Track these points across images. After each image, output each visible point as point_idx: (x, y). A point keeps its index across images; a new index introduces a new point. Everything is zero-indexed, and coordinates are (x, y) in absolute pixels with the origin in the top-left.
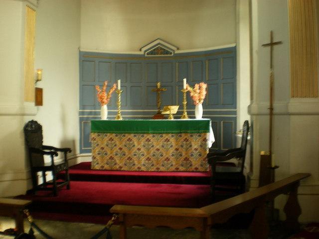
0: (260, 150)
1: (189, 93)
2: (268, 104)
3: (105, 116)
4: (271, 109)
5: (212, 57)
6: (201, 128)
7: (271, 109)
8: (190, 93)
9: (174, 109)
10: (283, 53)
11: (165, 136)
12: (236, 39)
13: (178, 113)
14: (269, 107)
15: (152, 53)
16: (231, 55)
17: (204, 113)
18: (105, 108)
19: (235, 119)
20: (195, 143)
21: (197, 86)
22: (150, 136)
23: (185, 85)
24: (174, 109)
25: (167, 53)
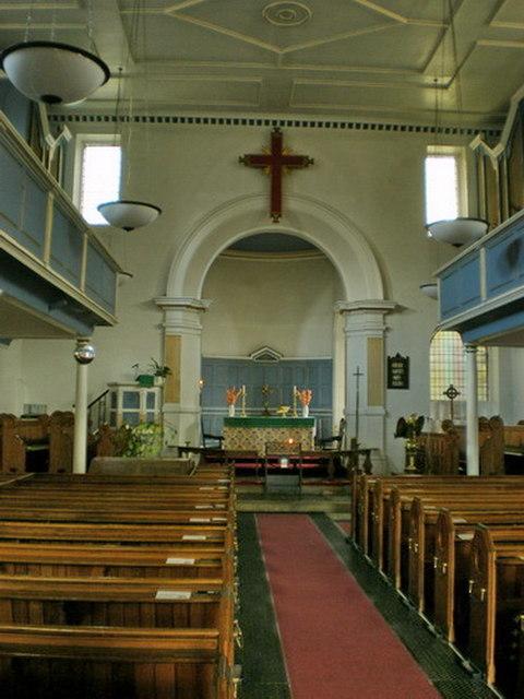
0: (350, 434)
1: (298, 397)
2: (214, 434)
3: (232, 415)
4: (357, 412)
5: (311, 366)
6: (308, 423)
7: (357, 412)
8: (451, 422)
9: (286, 409)
10: (364, 380)
11: (282, 430)
12: (333, 352)
13: (289, 411)
14: (439, 107)
15: (259, 358)
16: (328, 366)
17: (310, 412)
18: (307, 409)
19: (331, 418)
20: (304, 435)
21: (304, 393)
22: (270, 430)
23: (295, 391)
24: (286, 409)
25: (273, 359)
